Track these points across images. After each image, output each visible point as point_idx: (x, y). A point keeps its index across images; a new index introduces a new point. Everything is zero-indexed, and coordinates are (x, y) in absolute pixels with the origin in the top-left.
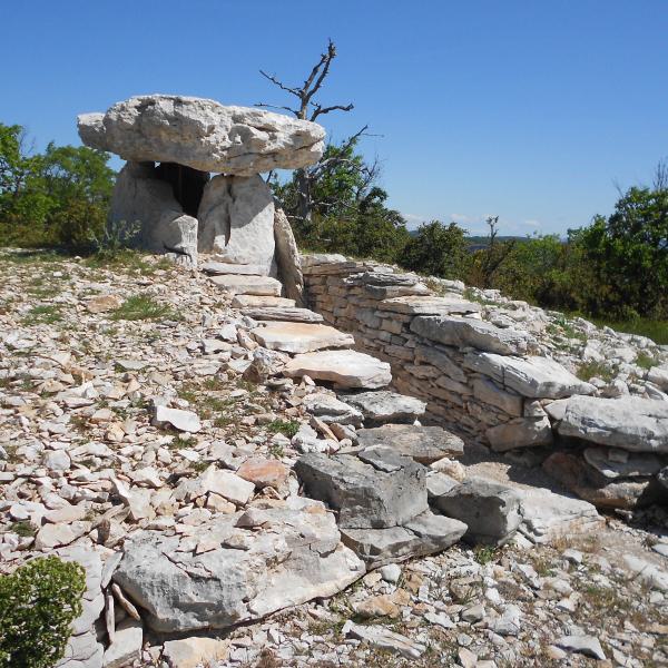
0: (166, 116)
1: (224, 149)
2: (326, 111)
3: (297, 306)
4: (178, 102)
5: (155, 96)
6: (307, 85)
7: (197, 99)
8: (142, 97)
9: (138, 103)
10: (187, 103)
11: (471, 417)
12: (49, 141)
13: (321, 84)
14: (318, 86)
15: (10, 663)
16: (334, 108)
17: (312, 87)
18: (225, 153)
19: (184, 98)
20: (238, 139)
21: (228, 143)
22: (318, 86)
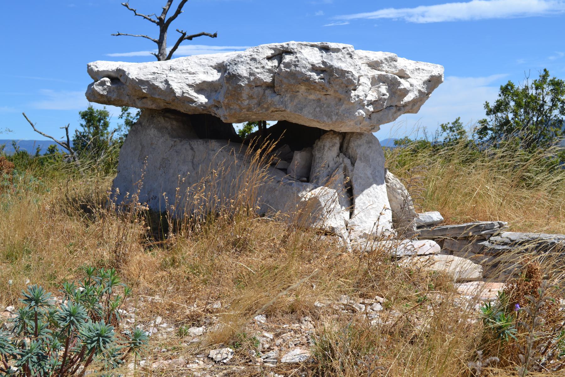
0: (314, 69)
1: (371, 103)
2: (190, 38)
3: (261, 149)
4: (326, 49)
5: (293, 44)
6: (165, 12)
7: (344, 45)
8: (273, 45)
9: (270, 53)
10: (337, 50)
11: (547, 199)
12: (79, 125)
13: (182, 10)
14: (178, 12)
15: (128, 191)
16: (207, 35)
17: (171, 14)
18: (371, 108)
19: (332, 45)
20: (383, 89)
21: (373, 96)
22: (178, 12)
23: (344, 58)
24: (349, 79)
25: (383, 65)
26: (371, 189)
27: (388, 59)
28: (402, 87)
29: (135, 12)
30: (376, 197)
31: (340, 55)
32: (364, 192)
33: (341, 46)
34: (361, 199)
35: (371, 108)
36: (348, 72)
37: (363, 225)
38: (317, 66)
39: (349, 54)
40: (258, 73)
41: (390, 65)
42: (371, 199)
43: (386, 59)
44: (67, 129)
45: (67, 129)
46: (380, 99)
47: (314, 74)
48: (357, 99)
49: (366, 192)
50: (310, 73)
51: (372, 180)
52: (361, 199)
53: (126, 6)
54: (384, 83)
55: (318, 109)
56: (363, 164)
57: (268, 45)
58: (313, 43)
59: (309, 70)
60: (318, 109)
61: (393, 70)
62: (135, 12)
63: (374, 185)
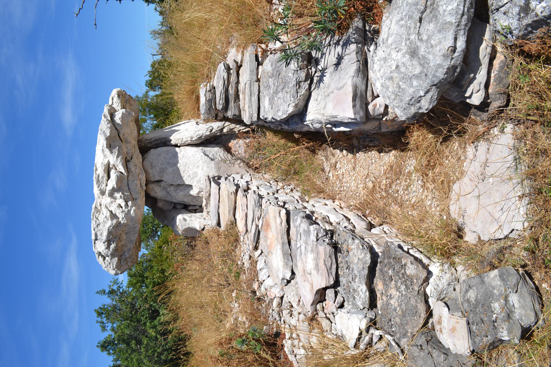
18: (130, 203)
23: (100, 230)
24: (113, 228)
25: (102, 188)
26: (180, 168)
27: (98, 185)
28: (115, 186)
29: (80, 9)
30: (186, 165)
31: (99, 234)
32: (182, 175)
33: (93, 233)
34: (186, 179)
35: (130, 203)
36: (109, 230)
37: (202, 180)
38: (106, 246)
39: (97, 226)
40: (113, 267)
41: (102, 182)
42: (187, 169)
43: (98, 187)
44: (153, 55)
45: (153, 55)
46: (124, 199)
47: (111, 246)
48: (124, 219)
49: (182, 173)
50: (111, 249)
51: (175, 168)
52: (186, 179)
53: (77, 15)
54: (113, 194)
55: (132, 233)
56: (165, 175)
57: (97, 258)
58: (93, 244)
59: (109, 250)
60: (132, 233)
61: (105, 179)
62: (80, 9)
63: (179, 165)
